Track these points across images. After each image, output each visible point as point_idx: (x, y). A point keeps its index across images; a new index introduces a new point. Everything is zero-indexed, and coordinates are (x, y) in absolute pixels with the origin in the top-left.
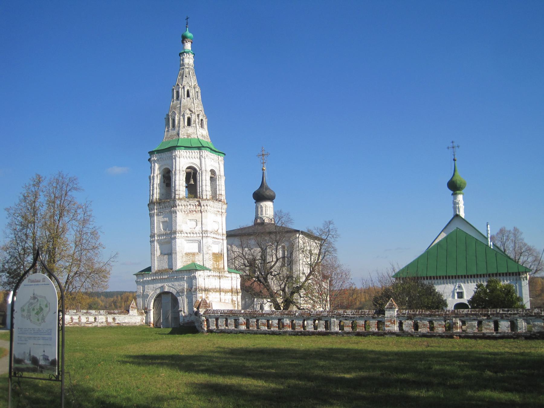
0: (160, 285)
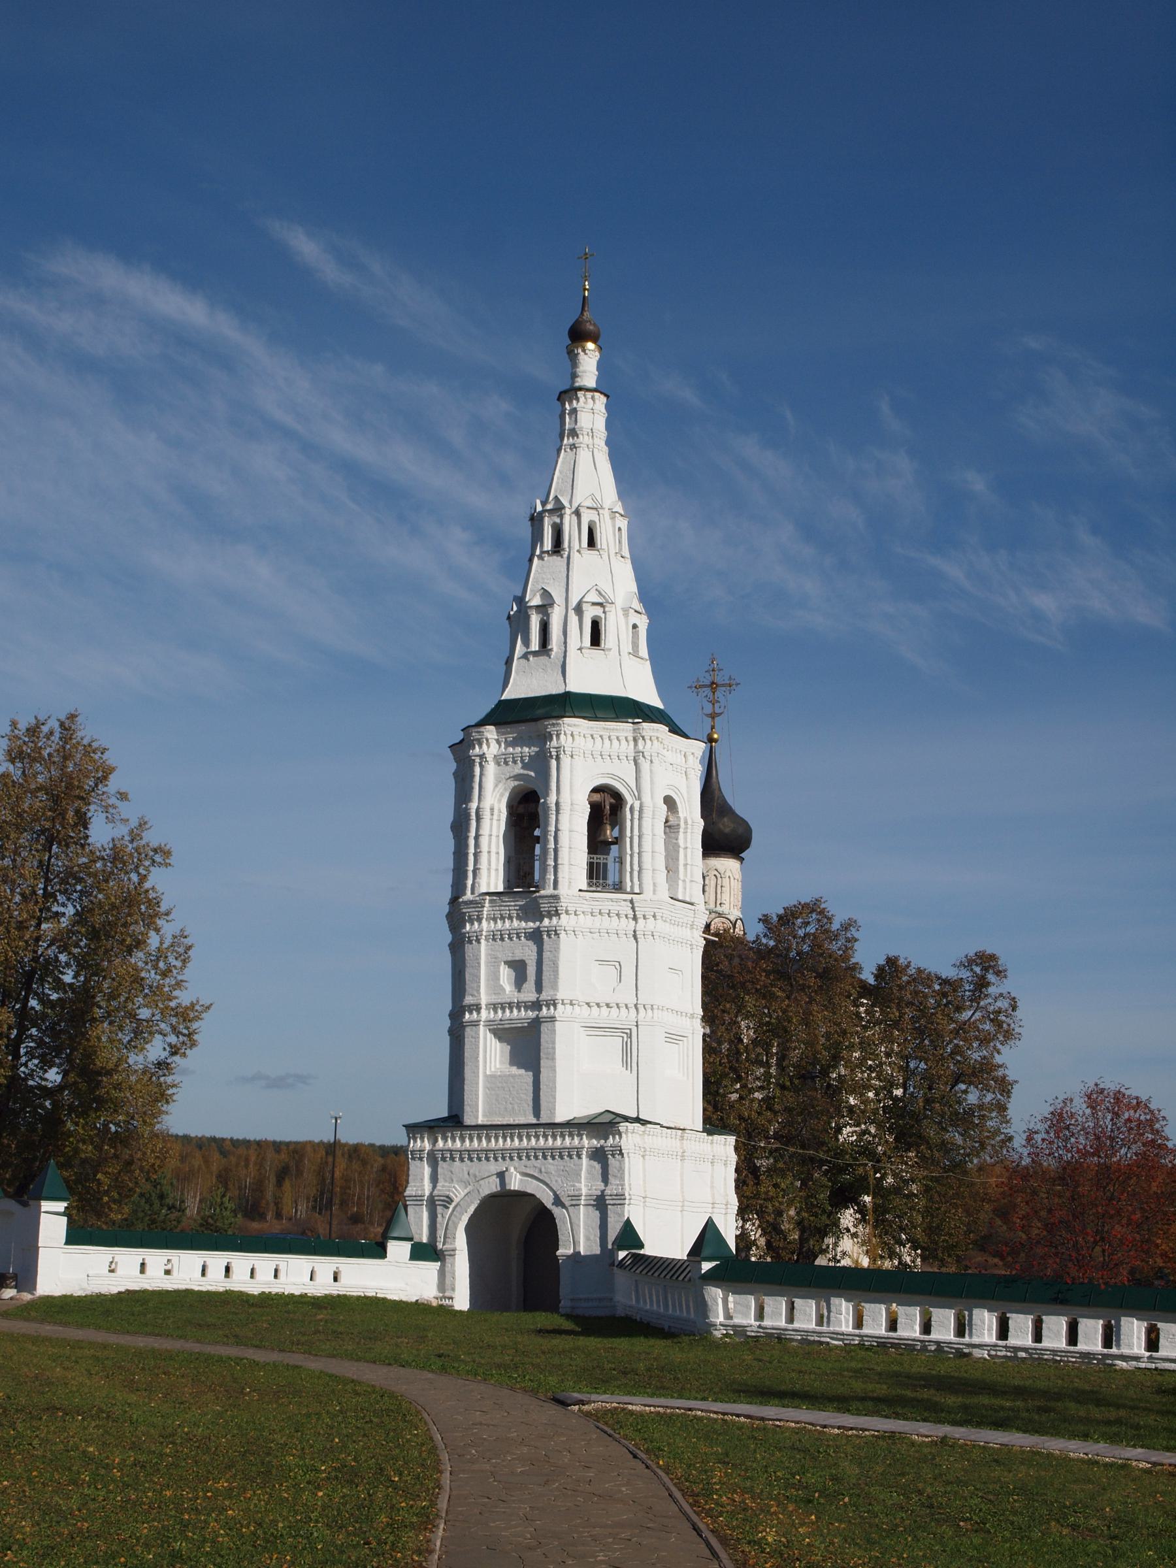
0: (494, 1167)
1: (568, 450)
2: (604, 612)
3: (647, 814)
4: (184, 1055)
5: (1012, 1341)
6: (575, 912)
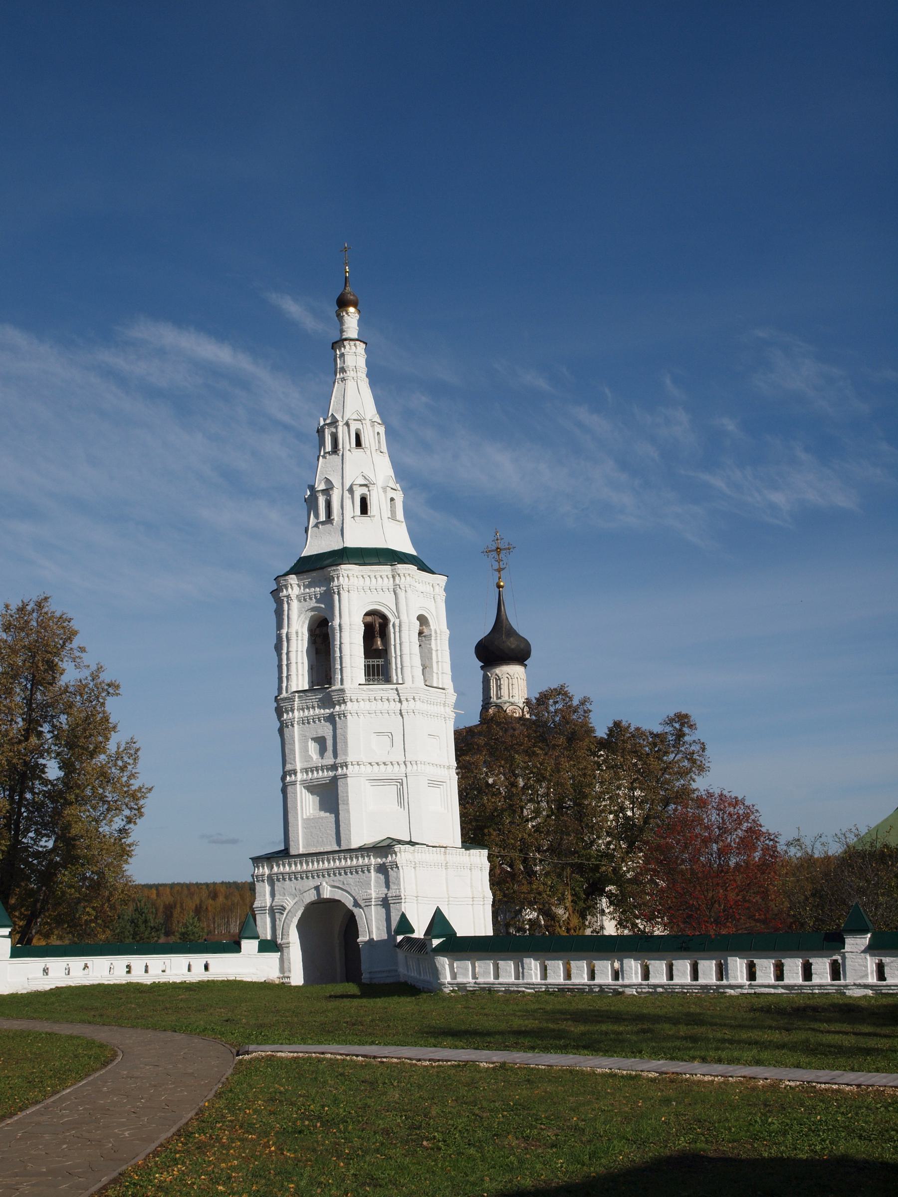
0: (312, 883)
1: (340, 382)
2: (369, 491)
3: (405, 628)
4: (135, 823)
5: (653, 981)
6: (357, 700)
